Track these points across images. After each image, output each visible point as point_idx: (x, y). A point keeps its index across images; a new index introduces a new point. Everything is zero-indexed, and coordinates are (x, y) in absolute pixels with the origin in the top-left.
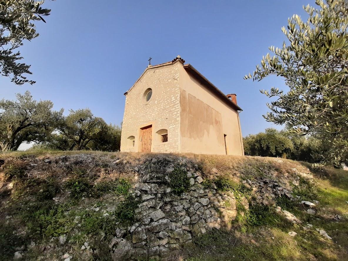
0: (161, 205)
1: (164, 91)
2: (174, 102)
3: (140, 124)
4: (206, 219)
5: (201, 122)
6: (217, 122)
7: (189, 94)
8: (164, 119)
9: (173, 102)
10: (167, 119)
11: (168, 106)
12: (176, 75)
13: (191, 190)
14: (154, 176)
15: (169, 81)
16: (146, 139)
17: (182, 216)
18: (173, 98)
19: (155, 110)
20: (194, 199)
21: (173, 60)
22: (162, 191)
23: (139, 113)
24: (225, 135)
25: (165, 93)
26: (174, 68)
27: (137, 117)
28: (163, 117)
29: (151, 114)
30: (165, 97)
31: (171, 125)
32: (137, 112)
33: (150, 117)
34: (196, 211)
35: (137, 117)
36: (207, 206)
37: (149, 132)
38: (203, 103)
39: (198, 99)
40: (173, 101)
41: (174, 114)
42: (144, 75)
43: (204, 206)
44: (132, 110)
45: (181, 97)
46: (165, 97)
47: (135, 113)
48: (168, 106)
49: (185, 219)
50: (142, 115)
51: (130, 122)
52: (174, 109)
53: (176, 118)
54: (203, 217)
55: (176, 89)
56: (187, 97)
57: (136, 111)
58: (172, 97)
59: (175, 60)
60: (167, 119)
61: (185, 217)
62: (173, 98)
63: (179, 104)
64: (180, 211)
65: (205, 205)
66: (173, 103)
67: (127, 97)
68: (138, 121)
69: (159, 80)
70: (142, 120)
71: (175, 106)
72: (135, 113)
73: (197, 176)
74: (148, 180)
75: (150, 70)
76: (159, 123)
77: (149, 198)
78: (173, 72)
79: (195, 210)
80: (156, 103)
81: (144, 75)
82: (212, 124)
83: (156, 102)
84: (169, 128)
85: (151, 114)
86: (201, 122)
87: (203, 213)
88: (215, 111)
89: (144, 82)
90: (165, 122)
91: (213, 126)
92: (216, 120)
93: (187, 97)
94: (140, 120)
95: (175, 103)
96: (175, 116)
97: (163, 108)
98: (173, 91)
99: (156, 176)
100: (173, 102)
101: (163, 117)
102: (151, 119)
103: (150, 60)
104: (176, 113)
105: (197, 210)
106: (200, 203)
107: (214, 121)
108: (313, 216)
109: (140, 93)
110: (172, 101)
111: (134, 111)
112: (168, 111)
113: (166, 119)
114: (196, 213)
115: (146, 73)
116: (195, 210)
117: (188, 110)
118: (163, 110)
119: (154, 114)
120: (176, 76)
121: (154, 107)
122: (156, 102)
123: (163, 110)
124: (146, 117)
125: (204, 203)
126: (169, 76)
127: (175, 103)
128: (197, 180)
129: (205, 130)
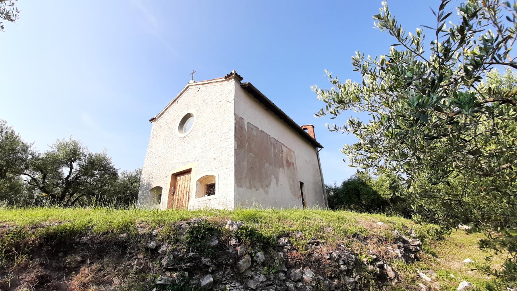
5: (267, 165)
6: (290, 164)
10: (215, 159)
15: (220, 103)
16: (181, 192)
24: (302, 184)
39: (262, 131)
47: (165, 150)
56: (246, 127)
59: (229, 76)
60: (215, 159)
69: (206, 102)
72: (165, 150)
74: (171, 265)
82: (283, 166)
86: (267, 165)
91: (284, 170)
92: (287, 161)
93: (246, 127)
103: (193, 74)
107: (285, 162)
112: (216, 148)
117: (247, 146)
129: (273, 176)
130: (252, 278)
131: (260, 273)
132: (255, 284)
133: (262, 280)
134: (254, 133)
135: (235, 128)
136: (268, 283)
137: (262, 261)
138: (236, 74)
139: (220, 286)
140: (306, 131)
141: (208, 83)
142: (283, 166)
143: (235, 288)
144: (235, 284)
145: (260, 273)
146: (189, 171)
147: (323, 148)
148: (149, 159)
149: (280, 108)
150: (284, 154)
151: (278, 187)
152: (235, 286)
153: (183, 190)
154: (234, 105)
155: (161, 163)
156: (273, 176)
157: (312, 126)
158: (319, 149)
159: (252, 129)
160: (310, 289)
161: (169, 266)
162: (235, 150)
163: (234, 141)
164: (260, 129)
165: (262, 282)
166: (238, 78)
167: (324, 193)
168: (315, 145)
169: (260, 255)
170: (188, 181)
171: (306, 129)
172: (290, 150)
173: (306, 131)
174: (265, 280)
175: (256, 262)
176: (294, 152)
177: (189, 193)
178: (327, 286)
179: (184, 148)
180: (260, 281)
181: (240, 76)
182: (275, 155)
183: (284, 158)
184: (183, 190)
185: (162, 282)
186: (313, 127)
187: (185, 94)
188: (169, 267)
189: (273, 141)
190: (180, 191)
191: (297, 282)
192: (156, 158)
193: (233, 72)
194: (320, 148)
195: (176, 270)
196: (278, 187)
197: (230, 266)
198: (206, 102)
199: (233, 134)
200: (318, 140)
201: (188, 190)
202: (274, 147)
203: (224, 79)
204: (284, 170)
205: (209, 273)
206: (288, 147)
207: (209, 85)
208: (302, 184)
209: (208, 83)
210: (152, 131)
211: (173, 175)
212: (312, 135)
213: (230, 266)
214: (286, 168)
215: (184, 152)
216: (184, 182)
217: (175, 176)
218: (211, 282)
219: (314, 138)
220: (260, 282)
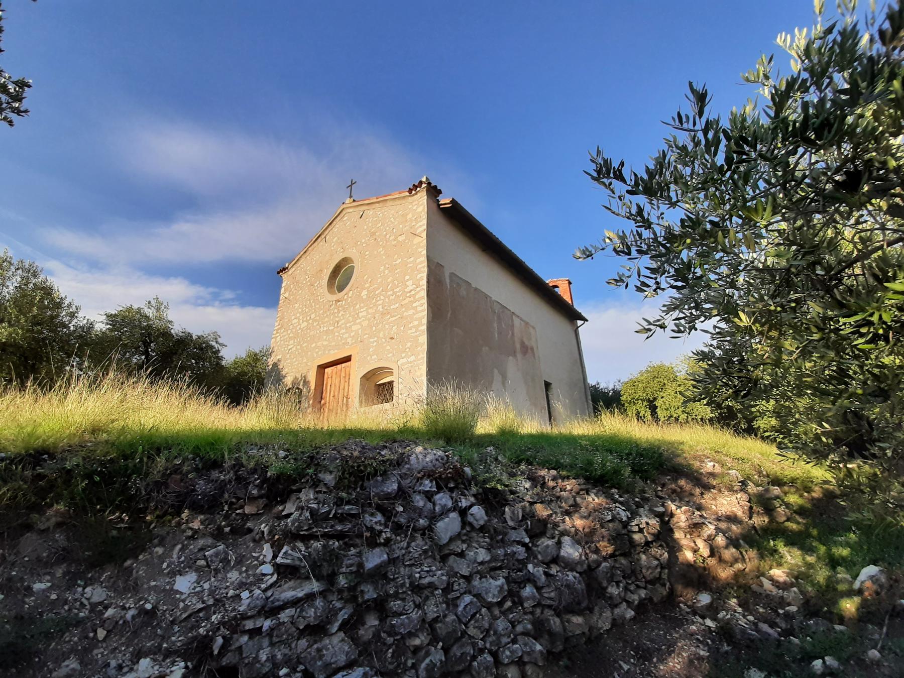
0: (343, 615)
1: (387, 266)
2: (413, 292)
3: (317, 353)
4: (497, 651)
5: (485, 349)
6: (526, 350)
7: (452, 275)
8: (384, 340)
9: (408, 295)
10: (392, 338)
11: (397, 305)
12: (418, 225)
13: (450, 555)
14: (329, 512)
15: (400, 239)
16: (334, 396)
17: (416, 650)
18: (410, 283)
19: (360, 315)
20: (459, 584)
21: (411, 187)
22: (351, 565)
23: (315, 324)
24: (547, 385)
25: (390, 271)
26: (415, 208)
27: (312, 333)
28: (381, 335)
29: (350, 327)
30: (389, 280)
31: (403, 355)
32: (310, 321)
33: (347, 335)
34: (466, 625)
35: (312, 333)
36: (500, 604)
37: (343, 375)
38: (489, 299)
39: (476, 289)
40: (411, 291)
41: (412, 325)
42: (334, 222)
43: (489, 606)
44: (298, 315)
45: (432, 280)
46: (389, 280)
47: (305, 324)
48: (397, 305)
49: (427, 661)
50: (325, 329)
51: (289, 347)
52: (411, 312)
53: (417, 336)
54: (488, 645)
55: (418, 261)
56: (448, 281)
57: (308, 318)
58: (408, 280)
59: (415, 187)
60: (392, 338)
61: (428, 654)
62: (410, 283)
63: (425, 301)
64: (409, 632)
65: (495, 600)
66: (410, 297)
67: (284, 276)
68: (314, 345)
69: (375, 237)
70: (325, 343)
71: (414, 305)
72: (305, 324)
73: (468, 505)
74: (306, 528)
75: (351, 210)
76: (371, 350)
77: (304, 592)
78: (410, 216)
79: (460, 621)
80: (365, 297)
81: (333, 225)
82: (514, 353)
83: (364, 293)
84: (399, 363)
85: (350, 327)
86: (485, 349)
87: (488, 631)
88: (521, 319)
89: (334, 240)
90: (388, 347)
91: (517, 360)
92: (523, 344)
93: (448, 281)
94: (319, 344)
95: (414, 296)
96: (414, 330)
97: (381, 310)
98: (409, 265)
99: (333, 512)
100: (408, 295)
101: (381, 335)
102: (349, 340)
103: (351, 186)
104: (416, 323)
105: (470, 620)
106: (478, 596)
107: (518, 346)
108: (345, 556)
109: (321, 271)
110: (407, 290)
111: (303, 318)
112: (394, 318)
113: (390, 340)
114: (464, 633)
115: (339, 218)
116: (460, 621)
117: (449, 315)
118: (383, 314)
119: (359, 327)
120: (418, 228)
121: (358, 306)
122: (364, 293)
123: (383, 314)
124: (336, 334)
125: (490, 595)
126: (401, 226)
127: (414, 296)
128: (470, 519)
129: (496, 371)
130: (462, 555)
131: (477, 546)
132: (468, 567)
133: (481, 559)
134: (463, 292)
135: (428, 282)
136: (494, 564)
137: (482, 523)
138: (429, 184)
139: (402, 569)
140: (556, 290)
141: (378, 202)
142: (515, 352)
143: (431, 573)
144: (430, 567)
145: (477, 546)
146: (348, 359)
147: (587, 321)
148: (278, 339)
149: (510, 248)
150: (516, 331)
151: (836, 22)
152: (430, 571)
153: (336, 394)
154: (425, 241)
155: (298, 347)
156: (496, 371)
157: (567, 282)
158: (579, 322)
159: (458, 284)
160: (575, 577)
161: (302, 531)
162: (428, 322)
163: (426, 306)
164: (473, 286)
165: (482, 563)
166: (434, 192)
167: (587, 401)
168: (572, 316)
169: (478, 513)
170: (345, 377)
171: (556, 287)
172: (527, 323)
173: (556, 290)
174: (488, 558)
175: (470, 524)
176: (534, 328)
177: (347, 398)
178: (607, 573)
179: (337, 319)
180: (479, 561)
181: (436, 187)
182: (500, 333)
183: (516, 339)
184: (336, 394)
185: (289, 561)
186: (570, 283)
187: (338, 225)
188: (302, 533)
189: (497, 308)
190: (332, 395)
191: (548, 564)
192: (290, 338)
193: (424, 180)
194: (583, 322)
195: (315, 537)
196: (836, 22)
197: (421, 532)
198: (375, 237)
199: (424, 293)
200: (578, 307)
201: (346, 394)
202: (499, 317)
203: (407, 194)
204: (517, 360)
205: (380, 545)
206: (524, 318)
207: (381, 204)
208: (547, 385)
209: (378, 202)
210: (282, 290)
211: (319, 366)
212: (567, 298)
213: (421, 532)
214: (519, 356)
215: (338, 327)
216: (338, 380)
217: (322, 368)
218: (383, 562)
219: (570, 302)
220: (478, 563)
